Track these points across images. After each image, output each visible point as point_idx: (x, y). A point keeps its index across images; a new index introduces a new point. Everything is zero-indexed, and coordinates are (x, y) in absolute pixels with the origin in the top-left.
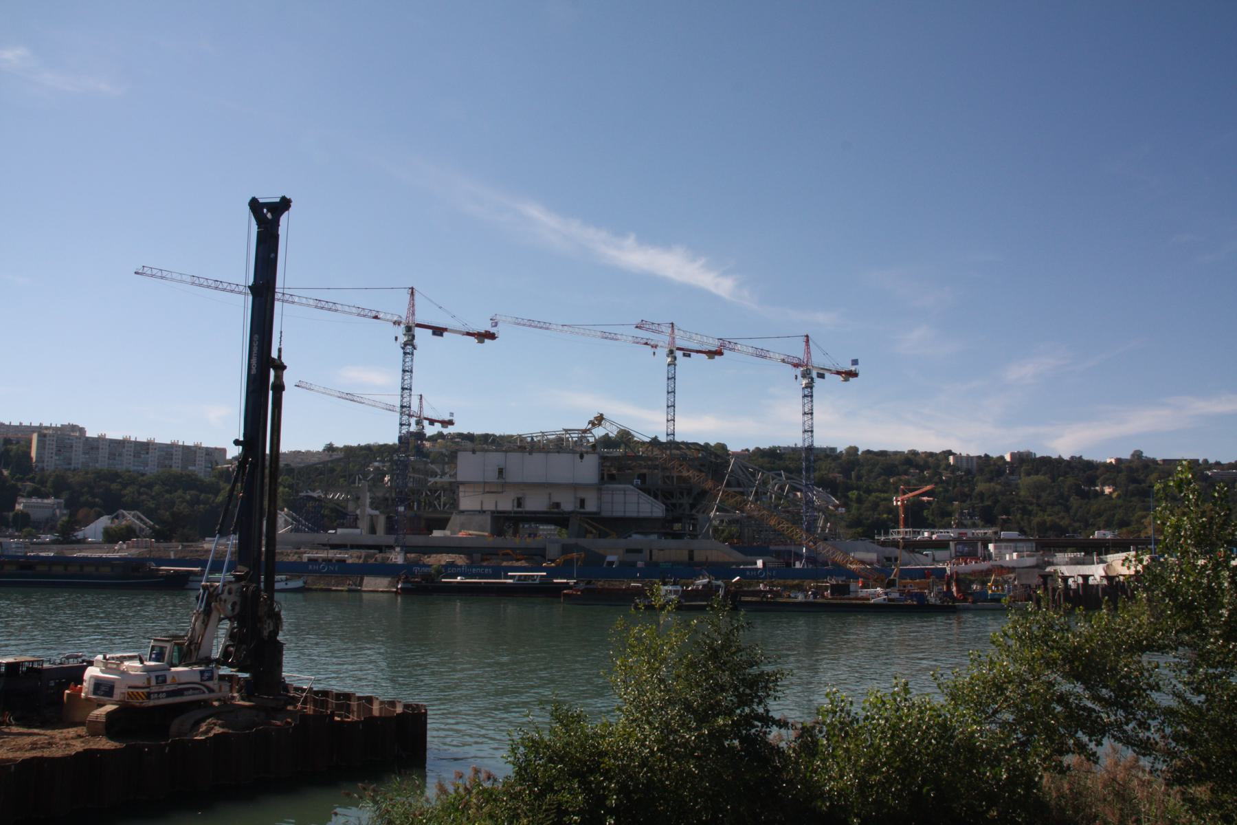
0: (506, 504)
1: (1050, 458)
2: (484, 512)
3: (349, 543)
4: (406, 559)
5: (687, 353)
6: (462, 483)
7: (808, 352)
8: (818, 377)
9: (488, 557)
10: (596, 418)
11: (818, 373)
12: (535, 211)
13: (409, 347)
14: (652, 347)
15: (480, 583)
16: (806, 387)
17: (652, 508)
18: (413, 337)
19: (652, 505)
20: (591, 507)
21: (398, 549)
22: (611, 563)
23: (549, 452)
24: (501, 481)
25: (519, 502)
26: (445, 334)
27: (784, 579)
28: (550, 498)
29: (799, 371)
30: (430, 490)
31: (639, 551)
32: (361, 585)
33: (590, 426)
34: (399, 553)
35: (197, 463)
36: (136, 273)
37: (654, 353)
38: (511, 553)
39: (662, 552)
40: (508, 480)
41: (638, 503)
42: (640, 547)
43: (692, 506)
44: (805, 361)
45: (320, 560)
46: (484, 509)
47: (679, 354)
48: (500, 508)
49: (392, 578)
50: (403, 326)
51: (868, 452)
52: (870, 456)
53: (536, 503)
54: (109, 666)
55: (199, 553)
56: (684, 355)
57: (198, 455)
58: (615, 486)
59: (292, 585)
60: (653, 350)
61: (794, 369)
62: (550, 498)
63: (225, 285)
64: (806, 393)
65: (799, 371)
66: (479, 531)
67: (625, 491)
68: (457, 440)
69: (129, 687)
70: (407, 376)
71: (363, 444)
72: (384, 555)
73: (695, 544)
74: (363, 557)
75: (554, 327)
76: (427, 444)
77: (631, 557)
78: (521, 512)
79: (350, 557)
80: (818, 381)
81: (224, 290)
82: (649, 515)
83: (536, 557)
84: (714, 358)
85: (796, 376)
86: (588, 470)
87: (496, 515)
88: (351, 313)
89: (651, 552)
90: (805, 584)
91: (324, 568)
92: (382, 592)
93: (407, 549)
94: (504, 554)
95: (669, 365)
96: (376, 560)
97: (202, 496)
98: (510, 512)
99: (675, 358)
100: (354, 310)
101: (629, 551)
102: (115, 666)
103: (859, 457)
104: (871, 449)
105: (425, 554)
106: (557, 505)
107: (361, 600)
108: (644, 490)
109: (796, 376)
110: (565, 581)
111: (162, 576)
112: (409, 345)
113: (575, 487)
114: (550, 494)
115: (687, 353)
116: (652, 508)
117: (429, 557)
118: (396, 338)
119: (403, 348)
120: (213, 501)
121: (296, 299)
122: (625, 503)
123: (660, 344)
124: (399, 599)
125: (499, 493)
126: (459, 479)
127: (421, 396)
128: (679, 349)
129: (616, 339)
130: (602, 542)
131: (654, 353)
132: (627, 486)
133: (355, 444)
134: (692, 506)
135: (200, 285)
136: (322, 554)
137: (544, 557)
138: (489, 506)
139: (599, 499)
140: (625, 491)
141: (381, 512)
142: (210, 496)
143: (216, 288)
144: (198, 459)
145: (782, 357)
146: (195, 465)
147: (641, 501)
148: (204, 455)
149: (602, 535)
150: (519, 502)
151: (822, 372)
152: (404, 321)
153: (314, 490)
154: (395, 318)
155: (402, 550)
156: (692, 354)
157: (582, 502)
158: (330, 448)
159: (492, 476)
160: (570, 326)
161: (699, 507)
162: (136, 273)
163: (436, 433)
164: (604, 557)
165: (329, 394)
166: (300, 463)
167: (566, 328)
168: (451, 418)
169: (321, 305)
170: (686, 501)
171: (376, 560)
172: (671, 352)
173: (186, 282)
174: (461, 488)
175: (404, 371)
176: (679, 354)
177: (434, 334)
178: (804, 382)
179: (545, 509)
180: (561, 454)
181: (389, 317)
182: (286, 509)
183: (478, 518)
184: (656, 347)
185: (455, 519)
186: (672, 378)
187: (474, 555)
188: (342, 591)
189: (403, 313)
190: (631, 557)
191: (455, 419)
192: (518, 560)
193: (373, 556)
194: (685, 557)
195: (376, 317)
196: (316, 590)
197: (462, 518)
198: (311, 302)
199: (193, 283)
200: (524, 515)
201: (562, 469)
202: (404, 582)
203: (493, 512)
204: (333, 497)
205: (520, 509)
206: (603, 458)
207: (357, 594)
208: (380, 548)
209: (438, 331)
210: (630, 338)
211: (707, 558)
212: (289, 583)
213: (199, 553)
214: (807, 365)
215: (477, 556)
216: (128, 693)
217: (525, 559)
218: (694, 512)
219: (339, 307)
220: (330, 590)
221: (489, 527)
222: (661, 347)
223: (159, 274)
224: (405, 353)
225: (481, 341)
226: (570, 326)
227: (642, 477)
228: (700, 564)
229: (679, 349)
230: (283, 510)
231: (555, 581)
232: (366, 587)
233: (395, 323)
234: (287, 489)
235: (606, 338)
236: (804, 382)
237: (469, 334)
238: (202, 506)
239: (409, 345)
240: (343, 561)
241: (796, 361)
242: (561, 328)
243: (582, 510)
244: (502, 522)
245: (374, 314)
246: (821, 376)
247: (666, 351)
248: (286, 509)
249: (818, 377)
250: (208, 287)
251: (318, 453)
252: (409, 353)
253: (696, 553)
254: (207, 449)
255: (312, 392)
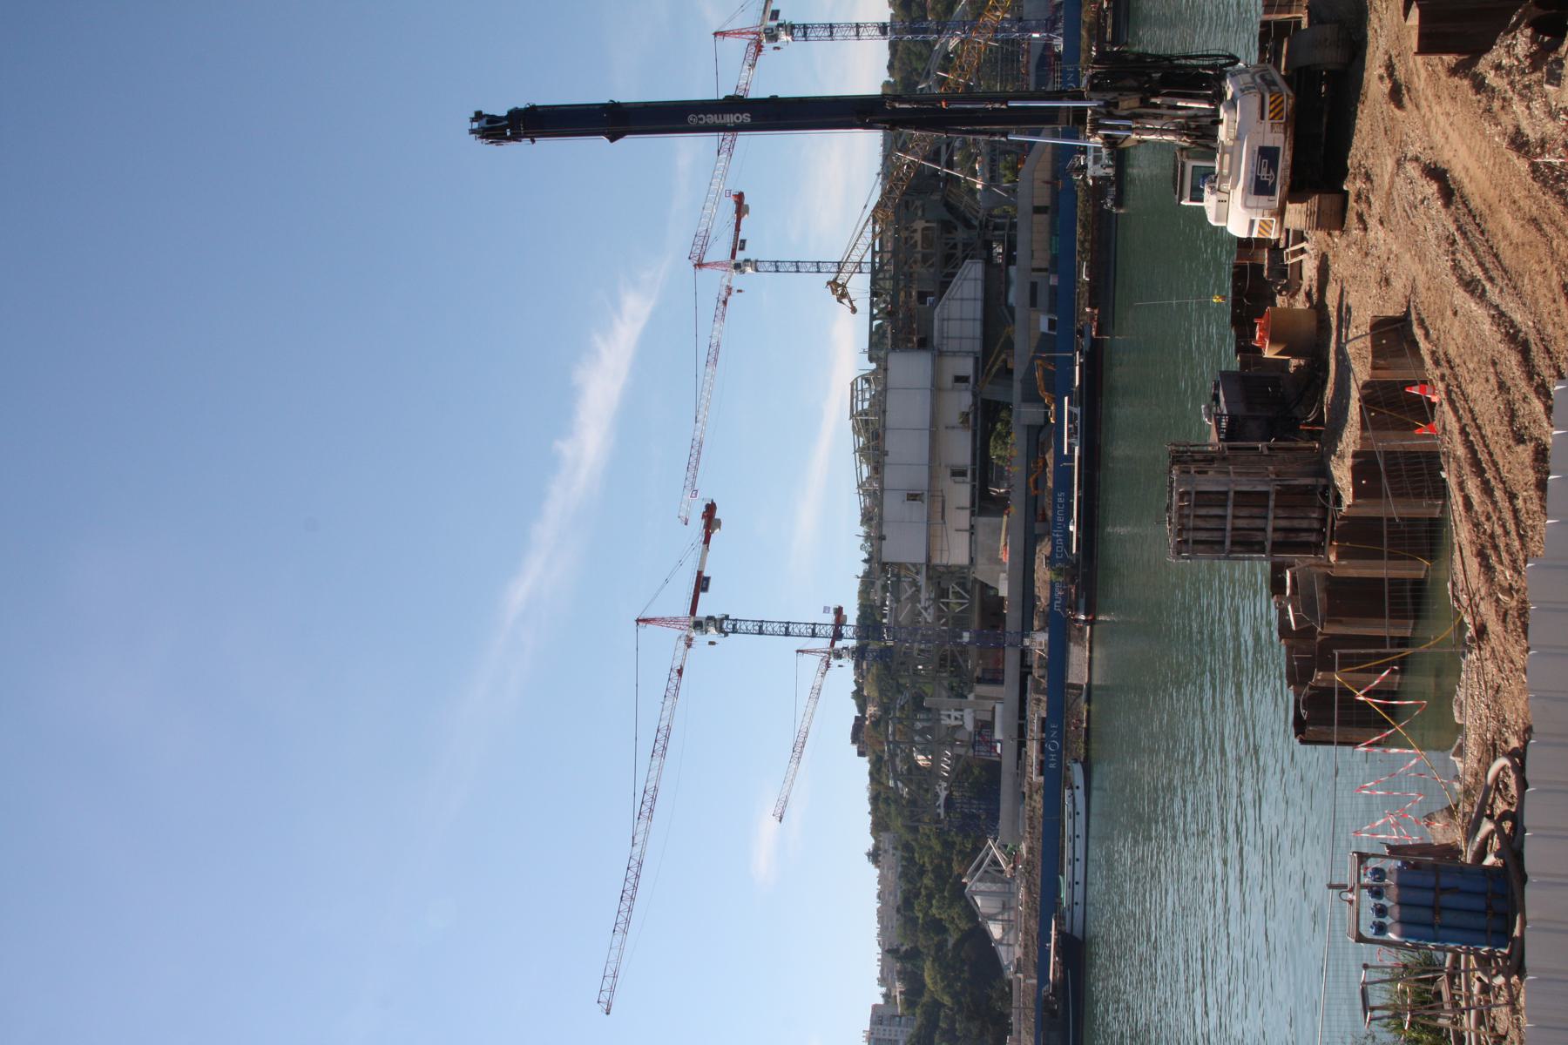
0: (961, 493)
1: (879, 911)
2: (972, 527)
3: (1015, 722)
4: (1041, 629)
5: (739, 245)
6: (929, 558)
7: (739, 33)
8: (776, 19)
9: (1040, 511)
10: (834, 291)
11: (771, 19)
12: (519, 593)
13: (725, 626)
14: (729, 294)
15: (1079, 498)
16: (792, 34)
17: (969, 280)
18: (710, 618)
19: (965, 279)
20: (966, 367)
21: (1027, 642)
22: (1052, 324)
23: (884, 426)
24: (927, 497)
25: (958, 473)
26: (705, 574)
27: (1080, 51)
28: (953, 428)
29: (768, 46)
30: (939, 618)
31: (1034, 286)
32: (1079, 687)
33: (845, 301)
34: (1033, 640)
35: (893, 1037)
36: (608, 1013)
37: (739, 291)
38: (1034, 476)
39: (1036, 255)
40: (926, 487)
41: (962, 299)
42: (1028, 287)
43: (968, 225)
44: (752, 37)
45: (1041, 757)
46: (967, 526)
47: (740, 256)
48: (966, 502)
49: (1070, 641)
50: (693, 634)
51: (891, 67)
52: (897, 64)
53: (960, 449)
54: (1226, 171)
55: (1030, 943)
56: (742, 248)
57: (881, 1036)
58: (936, 334)
59: (1078, 779)
60: (734, 293)
61: (763, 52)
62: (953, 428)
63: (628, 885)
64: (800, 34)
65: (768, 46)
66: (1000, 534)
67: (944, 320)
68: (865, 666)
69: (1262, 117)
70: (768, 628)
71: (869, 808)
72: (1035, 666)
73: (1024, 203)
74: (1037, 696)
75: (698, 433)
76: (871, 710)
77: (1043, 297)
78: (975, 418)
79: (1037, 712)
80: (782, 18)
81: (635, 887)
82: (979, 282)
83: (1041, 440)
84: (747, 206)
85: (775, 48)
86: (911, 368)
87: (976, 509)
88: (673, 708)
89: (1034, 270)
90: (1087, 20)
91: (1054, 746)
92: (1091, 651)
93: (1026, 628)
94: (1036, 488)
95: (757, 270)
96: (1043, 677)
97: (943, 1025)
98: (973, 487)
99: (747, 261)
100: (668, 703)
101: (1033, 302)
102: (1227, 157)
103: (898, 79)
104: (887, 63)
105: (1034, 606)
106: (965, 415)
107: (1100, 687)
108: (942, 293)
109: (775, 48)
110: (1077, 368)
111: (1064, 972)
112: (723, 625)
113: (936, 389)
114: (947, 428)
115: (739, 245)
116: (969, 280)
117: (1039, 598)
118: (712, 643)
119: (726, 634)
120: (949, 1008)
121: (651, 785)
122: (961, 319)
123: (725, 282)
124: (1101, 618)
125: (943, 502)
126: (922, 559)
127: (798, 651)
128: (733, 256)
129: (718, 346)
130: (1018, 339)
131: (739, 291)
132: (936, 317)
133: (869, 818)
134: (968, 225)
135: (628, 921)
136: (1033, 750)
137: (1040, 428)
138: (963, 519)
139: (954, 354)
140: (944, 320)
141: (971, 692)
142: (942, 1014)
143: (632, 899)
144: (887, 1037)
145: (746, 67)
146: (896, 1041)
147: (958, 296)
148: (882, 1028)
149: (1009, 344)
150: (958, 473)
151: (769, 15)
152: (686, 633)
153: (937, 796)
154: (682, 644)
155: (1028, 636)
156: (741, 237)
157: (959, 379)
158: (875, 856)
159: (919, 511)
160: (697, 411)
161: (968, 215)
162: (608, 1013)
163: (854, 701)
164: (1044, 334)
165: (794, 775)
166: (896, 896)
167: (700, 417)
168: (832, 611)
169: (661, 748)
170: (961, 234)
171: (1043, 677)
172: (737, 266)
173: (623, 942)
174: (936, 561)
175: (761, 632)
176: (740, 256)
177: (705, 589)
178: (784, 37)
179: (969, 434)
180: (888, 408)
181: (680, 653)
182: (964, 880)
183: (981, 536)
184: (729, 290)
185: (982, 573)
186: (777, 266)
187: (1036, 532)
188: (1089, 712)
189: (673, 635)
190: (1043, 297)
191: (833, 605)
192: (1045, 465)
193: (1037, 683)
194: (1043, 219)
195: (680, 672)
196: (1087, 750)
197: (982, 562)
198: (656, 763)
199: (625, 932)
200: (978, 466)
201: (909, 411)
202: (1077, 610)
203: (973, 514)
204: (946, 772)
205: (971, 380)
206: (896, 346)
207: (1095, 692)
208: (1025, 670)
209: (702, 584)
210: (717, 325)
211: (1047, 182)
212: (1076, 784)
213: (1030, 943)
214: (758, 34)
215: (1039, 528)
216: (1272, 119)
217: (1044, 454)
218: (976, 223)
219: (664, 724)
220: (1087, 730)
221: (994, 520)
222: (729, 281)
223: (610, 980)
224: (734, 631)
225: (718, 524)
226: (697, 411)
227: (922, 296)
228: (1055, 194)
229: (733, 256)
230: (966, 884)
231: (1077, 383)
232: (1082, 679)
233: (689, 646)
234: (934, 902)
235: (716, 360)
236: (784, 37)
237: (707, 541)
238: (957, 1026)
239: (723, 625)
240: (1044, 724)
241: (753, 49)
242: (699, 425)
243: (971, 380)
244: (985, 504)
245: (675, 675)
246: (775, 14)
247: (735, 273)
248: (964, 880)
249: (776, 19)
250: (630, 910)
251: (882, 880)
252: (734, 626)
253: (1039, 202)
254: (873, 1022)
255: (791, 797)
